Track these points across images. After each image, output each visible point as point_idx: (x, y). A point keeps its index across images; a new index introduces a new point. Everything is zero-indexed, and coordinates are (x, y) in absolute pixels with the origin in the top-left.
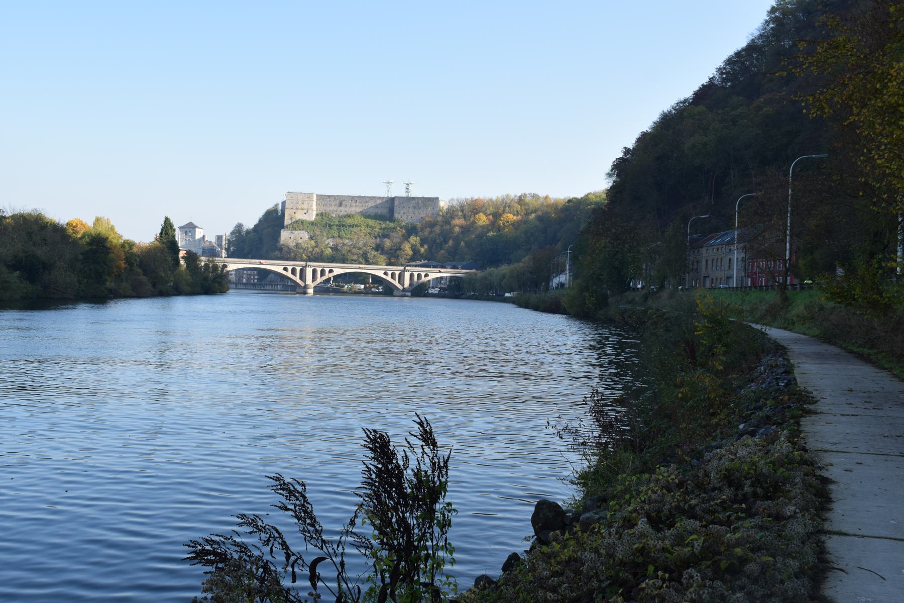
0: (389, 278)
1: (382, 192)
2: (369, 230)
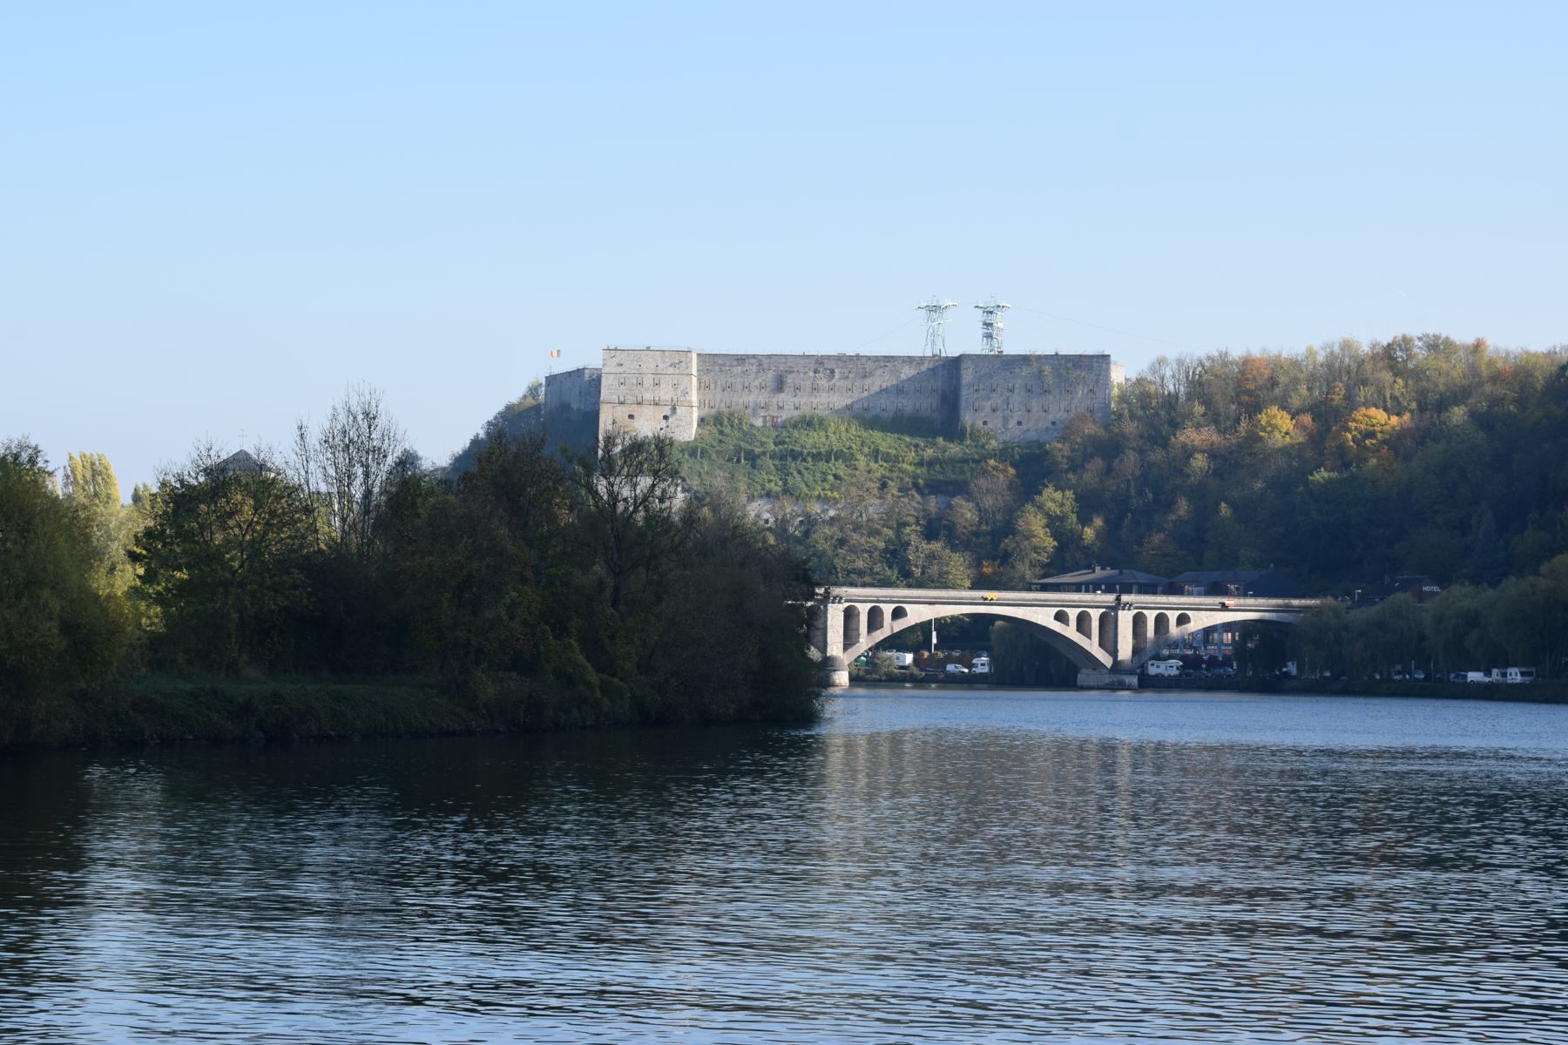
0: (1070, 632)
1: (912, 340)
2: (879, 470)
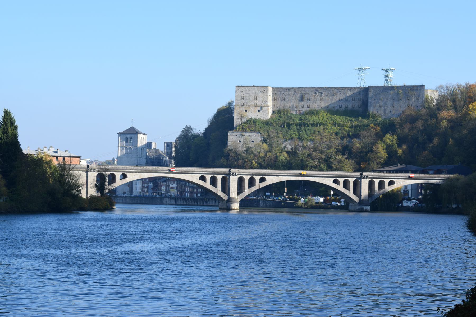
1: (353, 81)
2: (336, 129)
